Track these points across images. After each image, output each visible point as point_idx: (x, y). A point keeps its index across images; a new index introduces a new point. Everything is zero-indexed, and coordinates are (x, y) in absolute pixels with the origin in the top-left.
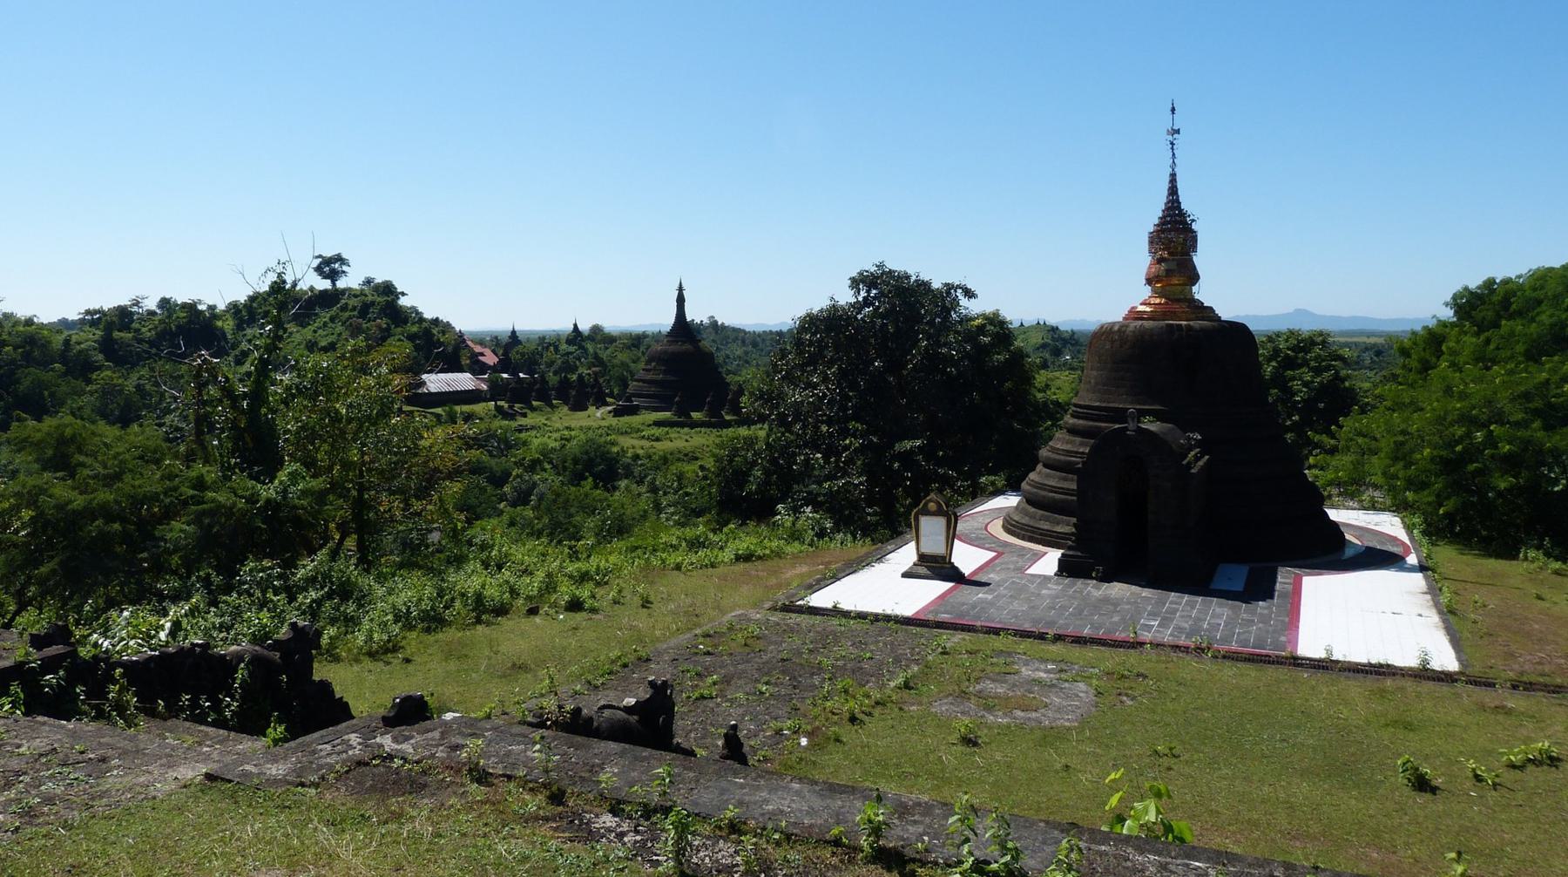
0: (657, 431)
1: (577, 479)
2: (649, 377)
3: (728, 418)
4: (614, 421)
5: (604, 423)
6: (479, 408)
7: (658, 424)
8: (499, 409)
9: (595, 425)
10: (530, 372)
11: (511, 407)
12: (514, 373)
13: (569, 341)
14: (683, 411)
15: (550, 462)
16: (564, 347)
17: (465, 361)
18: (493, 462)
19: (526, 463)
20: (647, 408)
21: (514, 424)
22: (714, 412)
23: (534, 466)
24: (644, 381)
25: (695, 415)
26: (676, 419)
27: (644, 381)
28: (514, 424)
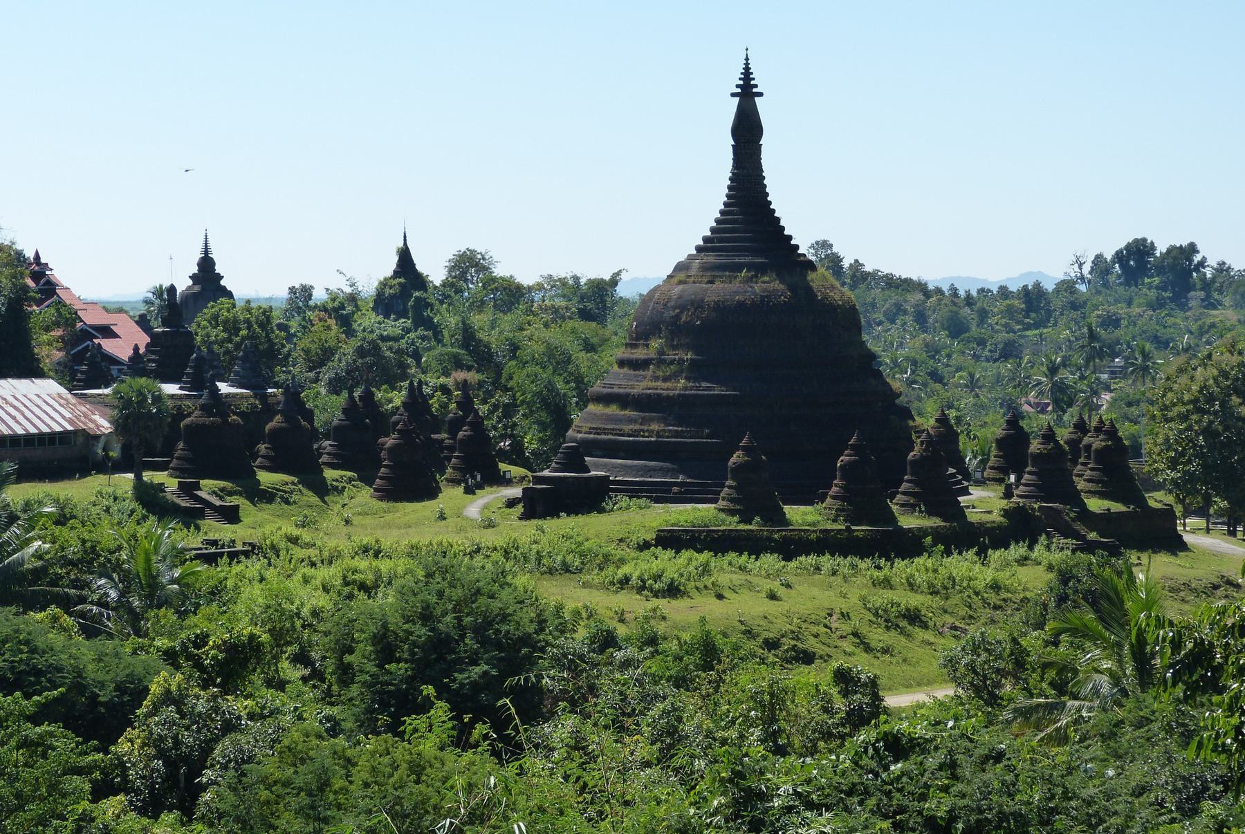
0: (670, 564)
1: (393, 708)
2: (643, 384)
3: (909, 522)
4: (526, 532)
5: (489, 538)
6: (81, 491)
7: (671, 540)
8: (150, 499)
9: (461, 542)
10: (255, 380)
11: (188, 489)
12: (200, 382)
13: (386, 302)
14: (759, 500)
15: (301, 658)
16: (367, 320)
17: (49, 351)
18: (84, 651)
19: (209, 654)
20: (633, 491)
21: (192, 540)
22: (866, 502)
23: (236, 665)
24: (623, 401)
25: (799, 515)
26: (732, 523)
27: (623, 401)
28: (192, 540)
